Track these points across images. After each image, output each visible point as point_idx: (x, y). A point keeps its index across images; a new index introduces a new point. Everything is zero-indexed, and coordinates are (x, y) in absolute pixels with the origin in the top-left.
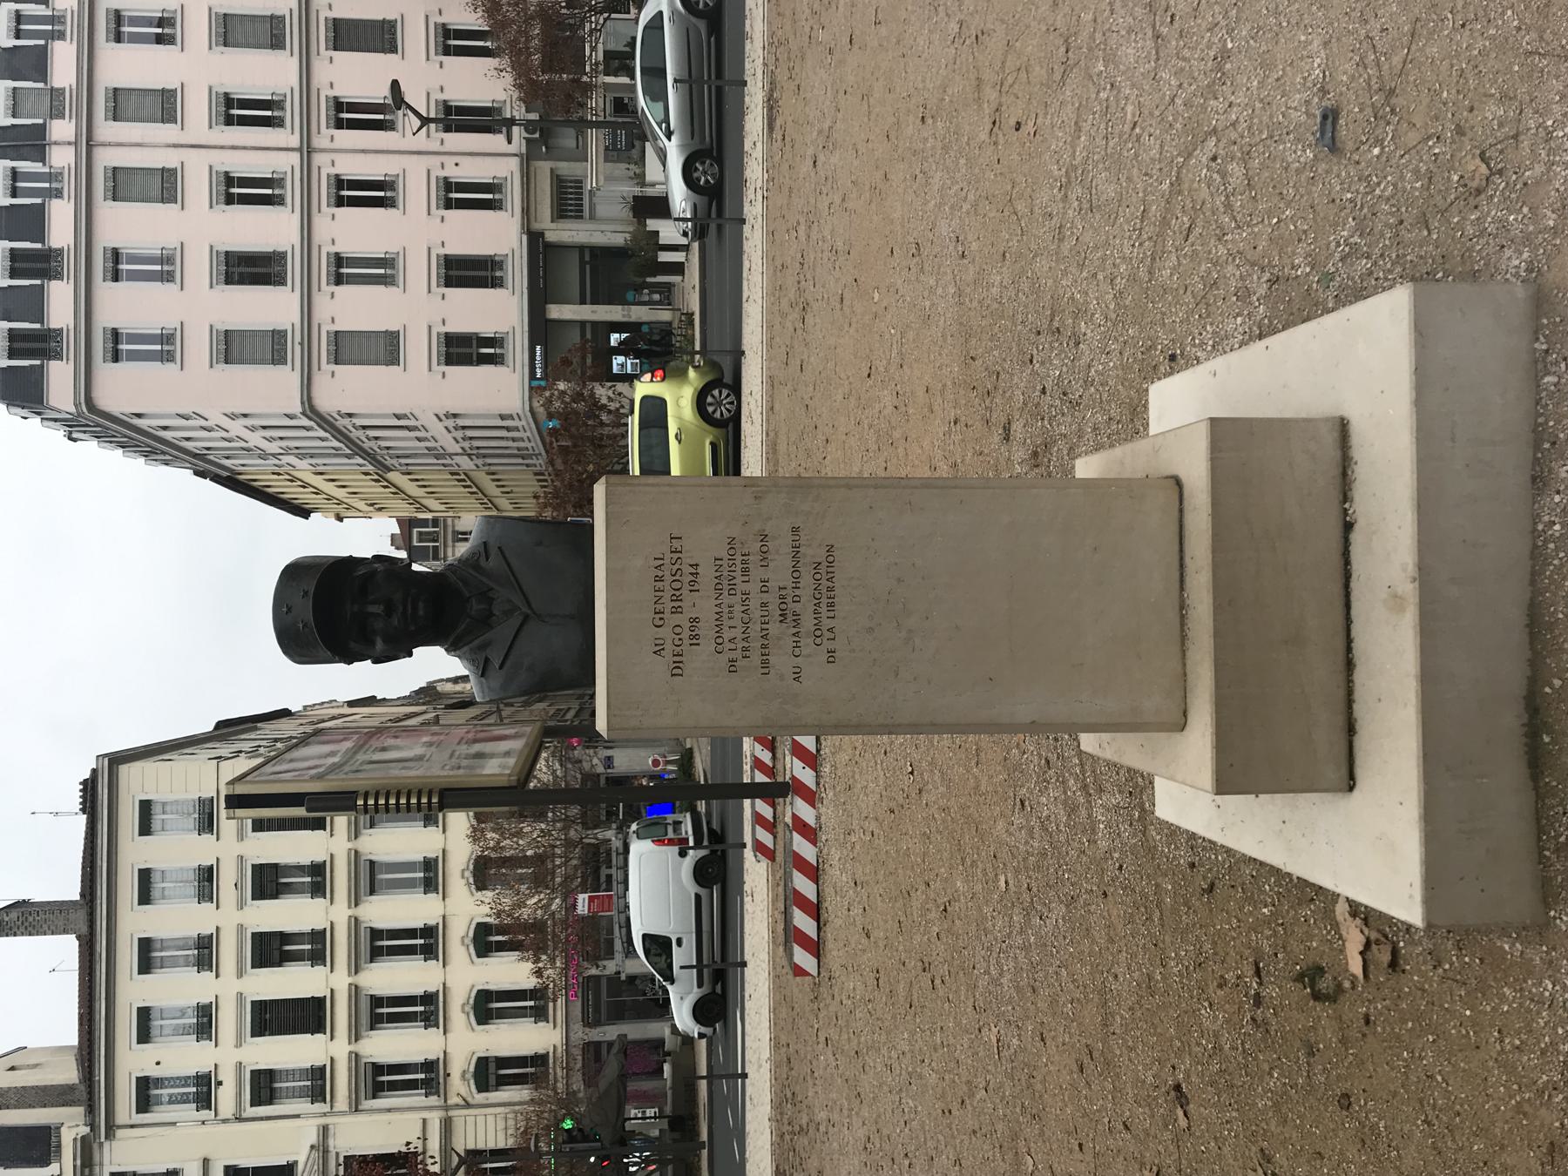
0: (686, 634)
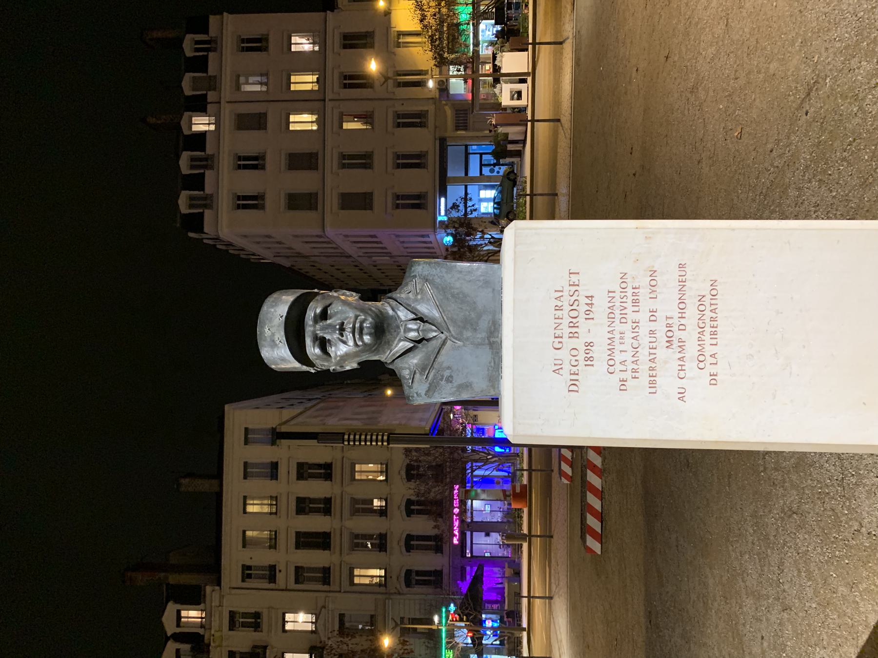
0: (581, 356)
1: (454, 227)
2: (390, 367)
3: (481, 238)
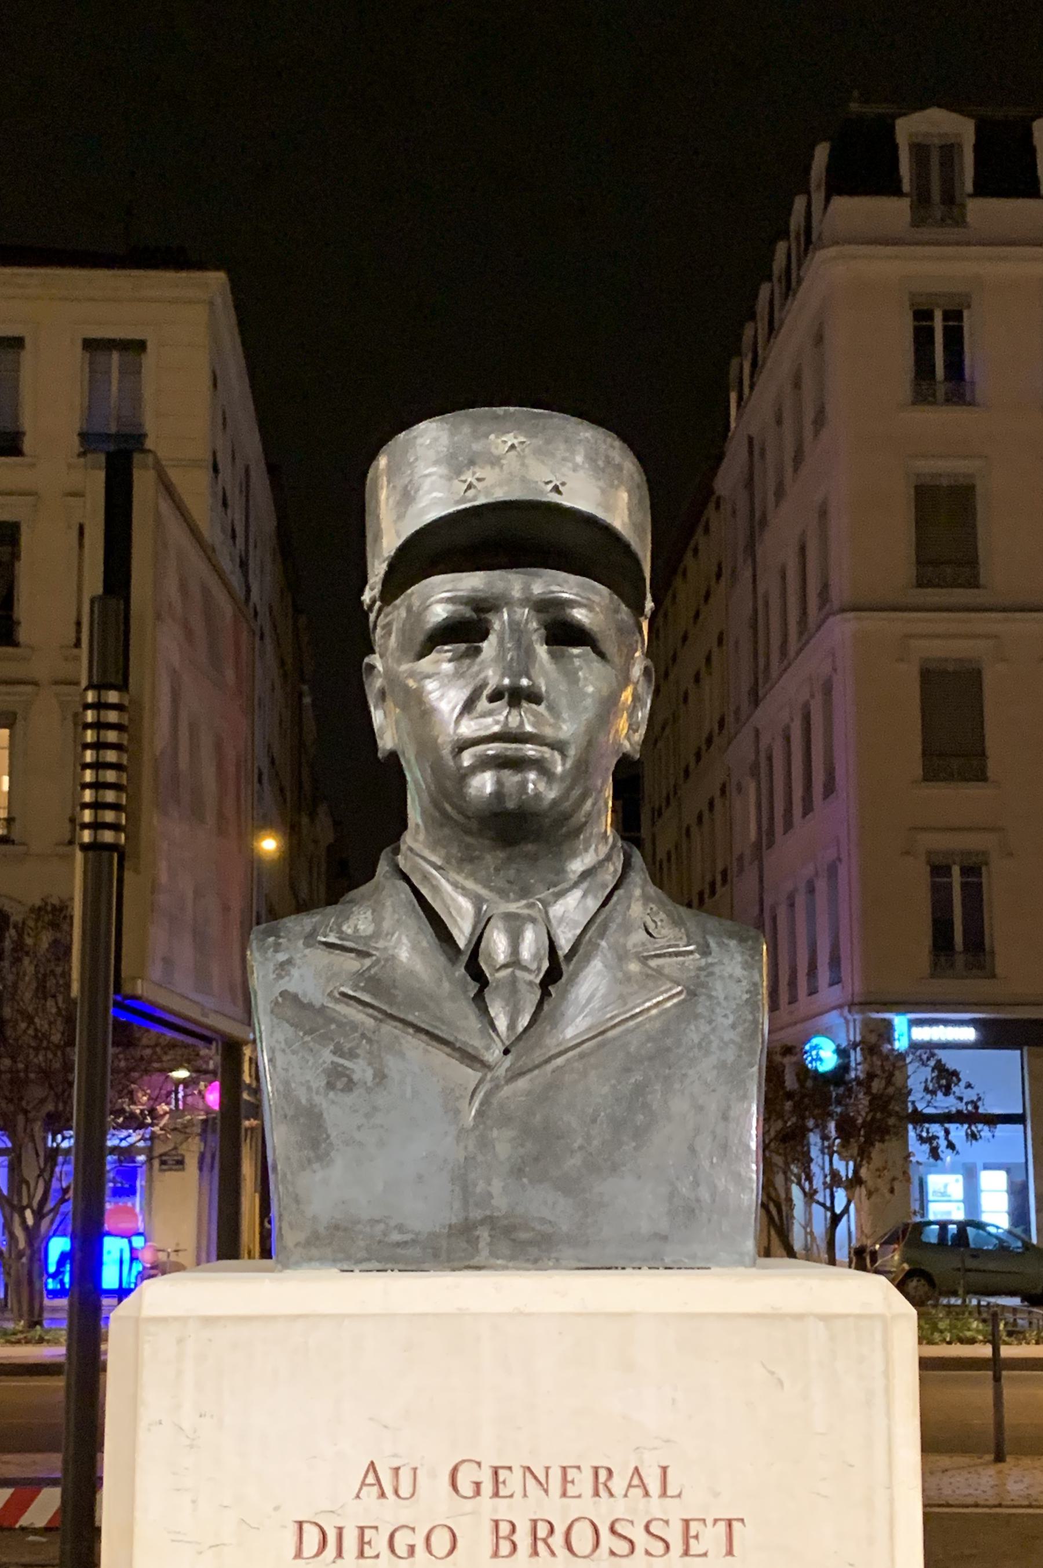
1: (871, 1076)
2: (383, 867)
3: (835, 1174)
